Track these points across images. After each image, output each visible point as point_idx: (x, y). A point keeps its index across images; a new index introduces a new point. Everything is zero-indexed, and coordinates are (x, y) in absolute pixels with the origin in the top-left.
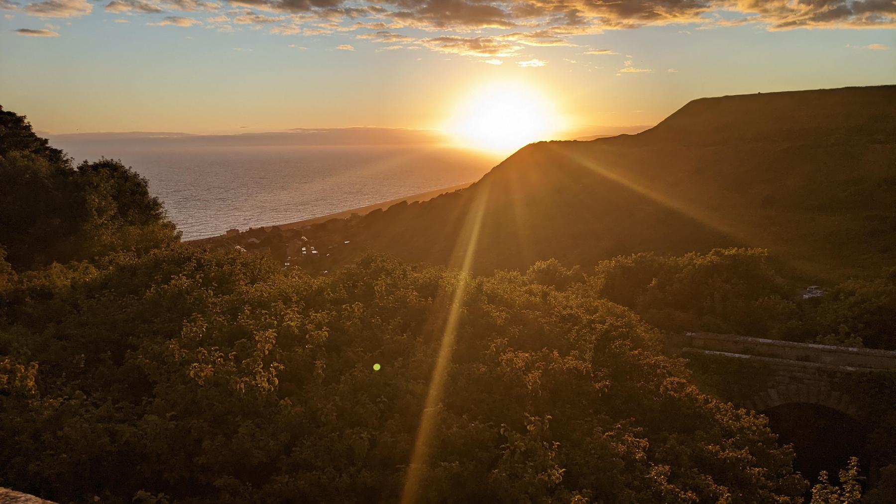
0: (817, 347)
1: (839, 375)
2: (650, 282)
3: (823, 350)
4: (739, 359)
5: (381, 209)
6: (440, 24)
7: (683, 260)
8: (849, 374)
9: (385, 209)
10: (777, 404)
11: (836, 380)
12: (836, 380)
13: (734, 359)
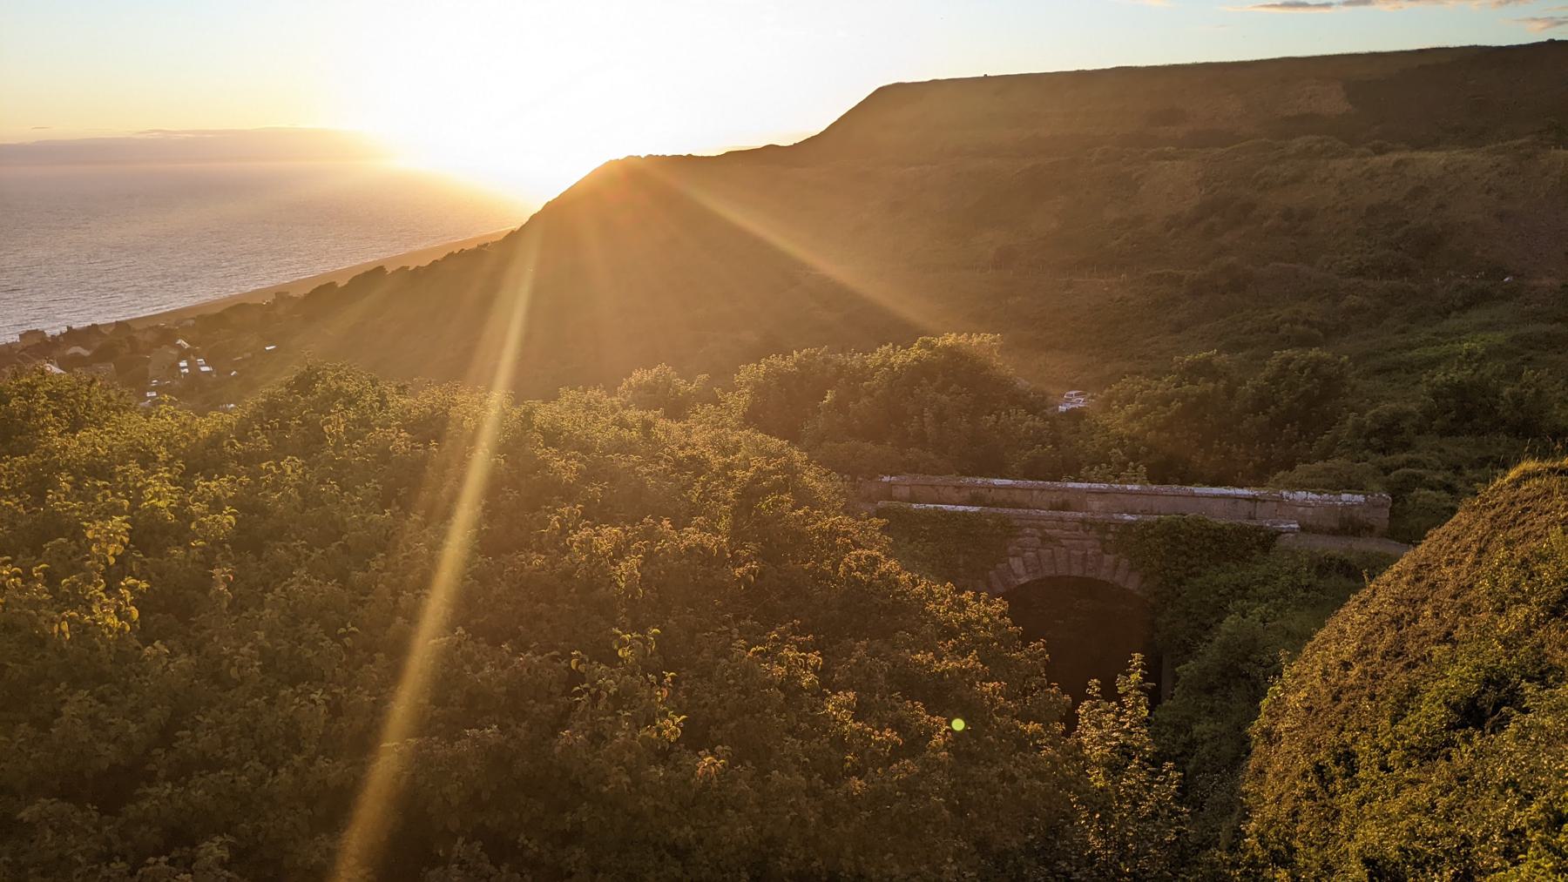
1: (1112, 528)
3: (1089, 492)
4: (965, 513)
5: (334, 283)
8: (1130, 524)
9: (341, 283)
10: (1023, 580)
11: (1110, 537)
12: (1110, 537)
13: (954, 514)
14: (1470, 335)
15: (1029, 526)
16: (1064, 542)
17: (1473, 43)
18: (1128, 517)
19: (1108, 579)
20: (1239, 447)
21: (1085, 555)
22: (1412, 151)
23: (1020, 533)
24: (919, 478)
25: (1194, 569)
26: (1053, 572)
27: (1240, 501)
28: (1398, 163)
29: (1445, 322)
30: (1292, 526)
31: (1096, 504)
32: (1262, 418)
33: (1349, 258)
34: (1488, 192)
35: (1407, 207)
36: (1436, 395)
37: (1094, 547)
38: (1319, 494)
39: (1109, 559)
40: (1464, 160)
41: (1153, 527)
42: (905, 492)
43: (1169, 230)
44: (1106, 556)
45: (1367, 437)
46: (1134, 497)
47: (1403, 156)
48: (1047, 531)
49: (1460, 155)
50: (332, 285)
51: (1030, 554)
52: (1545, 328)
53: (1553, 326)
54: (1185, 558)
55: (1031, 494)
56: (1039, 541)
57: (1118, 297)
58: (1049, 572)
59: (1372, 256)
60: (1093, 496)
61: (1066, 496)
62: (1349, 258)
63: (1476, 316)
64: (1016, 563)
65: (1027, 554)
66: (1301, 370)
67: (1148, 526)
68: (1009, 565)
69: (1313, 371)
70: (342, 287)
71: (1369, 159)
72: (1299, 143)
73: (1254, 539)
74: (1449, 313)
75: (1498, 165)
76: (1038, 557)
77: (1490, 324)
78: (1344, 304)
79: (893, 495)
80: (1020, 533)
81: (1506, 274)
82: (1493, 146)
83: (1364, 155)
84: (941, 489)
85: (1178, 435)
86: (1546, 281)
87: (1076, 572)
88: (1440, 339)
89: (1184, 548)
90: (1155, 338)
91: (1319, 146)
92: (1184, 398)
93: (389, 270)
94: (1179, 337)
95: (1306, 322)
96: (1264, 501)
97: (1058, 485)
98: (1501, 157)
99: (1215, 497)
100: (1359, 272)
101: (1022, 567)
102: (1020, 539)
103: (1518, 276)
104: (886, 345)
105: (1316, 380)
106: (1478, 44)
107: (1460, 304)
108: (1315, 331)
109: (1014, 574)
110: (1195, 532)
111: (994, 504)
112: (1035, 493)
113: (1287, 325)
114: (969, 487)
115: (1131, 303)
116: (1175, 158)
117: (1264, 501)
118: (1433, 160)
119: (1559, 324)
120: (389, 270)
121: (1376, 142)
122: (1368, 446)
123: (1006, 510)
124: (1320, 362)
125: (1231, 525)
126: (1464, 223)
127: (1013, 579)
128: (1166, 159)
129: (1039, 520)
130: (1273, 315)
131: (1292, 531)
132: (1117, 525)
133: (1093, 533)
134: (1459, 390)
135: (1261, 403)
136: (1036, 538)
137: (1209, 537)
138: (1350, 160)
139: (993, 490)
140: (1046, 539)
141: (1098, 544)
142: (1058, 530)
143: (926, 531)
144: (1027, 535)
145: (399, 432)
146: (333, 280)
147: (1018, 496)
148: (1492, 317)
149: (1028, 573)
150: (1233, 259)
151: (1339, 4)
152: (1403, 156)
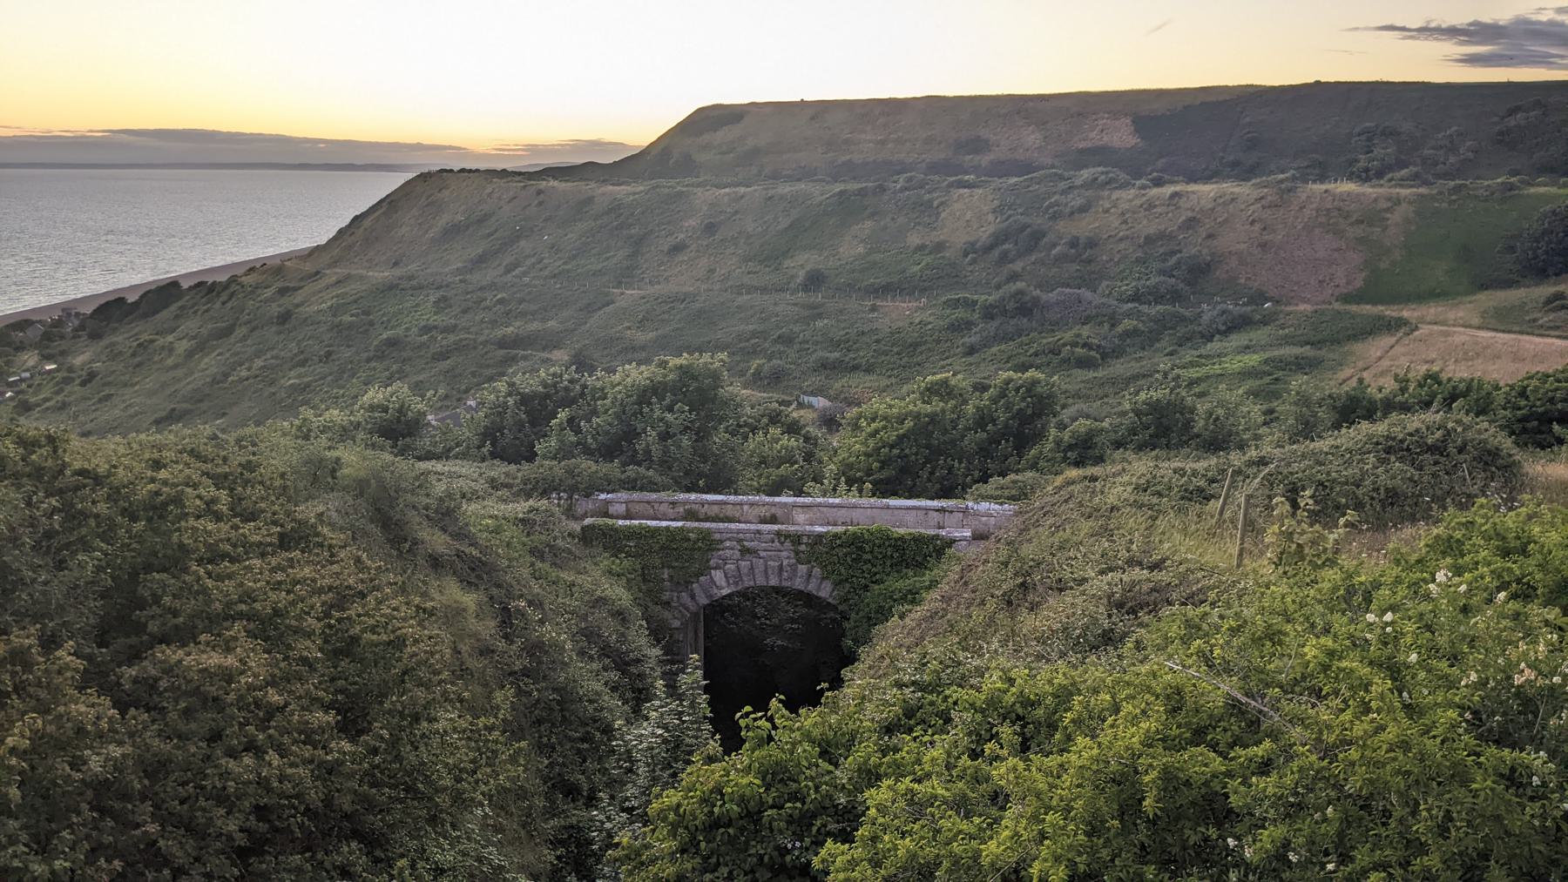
0: (1362, 306)
1: (805, 540)
2: (10, 397)
3: (795, 506)
4: (667, 528)
5: (123, 298)
6: (808, 272)
7: (1330, 442)
8: (820, 536)
9: (131, 298)
10: (725, 592)
11: (803, 548)
12: (803, 548)
13: (658, 529)
14: (1230, 357)
15: (729, 539)
16: (762, 554)
17: (1249, 83)
18: (818, 529)
19: (802, 587)
20: (960, 463)
21: (782, 564)
22: (1187, 183)
23: (721, 547)
24: (636, 496)
25: (878, 576)
26: (752, 583)
27: (930, 512)
28: (1175, 195)
29: (1209, 345)
30: (965, 534)
31: (800, 517)
32: (982, 435)
33: (1127, 285)
34: (1252, 223)
35: (1181, 236)
36: (1138, 413)
37: (788, 558)
38: (1001, 504)
39: (803, 568)
40: (1232, 193)
41: (840, 538)
42: (622, 509)
43: (967, 256)
44: (800, 566)
45: (1065, 451)
46: (836, 509)
47: (1178, 188)
48: (745, 543)
49: (1230, 187)
50: (121, 300)
51: (730, 567)
52: (1297, 351)
53: (1302, 350)
54: (869, 566)
55: (742, 509)
56: (738, 553)
57: (917, 321)
58: (748, 582)
59: (1148, 283)
60: (799, 510)
61: (773, 510)
62: (1127, 285)
63: (1237, 340)
64: (718, 576)
65: (728, 566)
66: (1017, 390)
67: (836, 536)
68: (711, 577)
69: (1029, 390)
70: (133, 303)
71: (1148, 190)
72: (1086, 174)
73: (931, 546)
74: (1213, 336)
75: (1262, 198)
76: (738, 568)
77: (1248, 347)
78: (1120, 329)
79: (610, 512)
80: (721, 547)
81: (1267, 300)
82: (1258, 180)
83: (1144, 187)
84: (656, 506)
85: (907, 451)
86: (1302, 307)
87: (774, 582)
88: (1203, 360)
89: (866, 557)
90: (949, 361)
91: (1103, 177)
92: (917, 416)
93: (185, 285)
94: (970, 359)
95: (1085, 345)
96: (952, 512)
97: (777, 499)
98: (1266, 190)
99: (908, 508)
100: (1136, 297)
101: (724, 579)
102: (721, 552)
103: (1278, 302)
104: (630, 364)
105: (1029, 399)
106: (1323, 80)
107: (1224, 328)
108: (1093, 353)
109: (717, 587)
110: (877, 541)
111: (707, 519)
112: (746, 507)
113: (1069, 347)
114: (684, 503)
115: (930, 327)
116: (974, 187)
117: (952, 512)
118: (1206, 191)
119: (1309, 347)
120: (185, 285)
121: (1155, 174)
122: (1065, 459)
123: (707, 525)
124: (1035, 382)
125: (910, 534)
126: (1230, 252)
127: (715, 591)
128: (965, 187)
129: (738, 533)
130: (1056, 338)
131: (964, 539)
132: (809, 536)
133: (788, 544)
134: (1155, 408)
135: (982, 420)
136: (737, 552)
137: (890, 546)
138: (1132, 191)
139: (706, 506)
140: (745, 551)
141: (792, 555)
142: (756, 543)
143: (631, 547)
144: (727, 548)
145: (980, 471)
146: (122, 296)
147: (729, 511)
148: (1251, 341)
149: (729, 585)
150: (1020, 285)
151: (1367, 29)
152: (1178, 188)
